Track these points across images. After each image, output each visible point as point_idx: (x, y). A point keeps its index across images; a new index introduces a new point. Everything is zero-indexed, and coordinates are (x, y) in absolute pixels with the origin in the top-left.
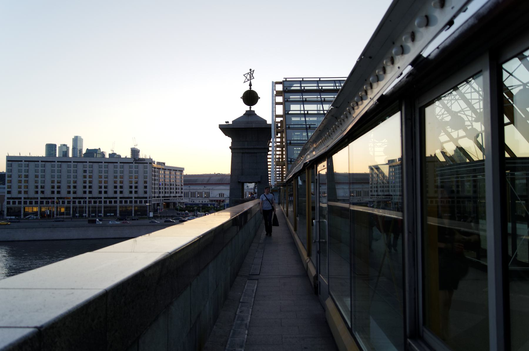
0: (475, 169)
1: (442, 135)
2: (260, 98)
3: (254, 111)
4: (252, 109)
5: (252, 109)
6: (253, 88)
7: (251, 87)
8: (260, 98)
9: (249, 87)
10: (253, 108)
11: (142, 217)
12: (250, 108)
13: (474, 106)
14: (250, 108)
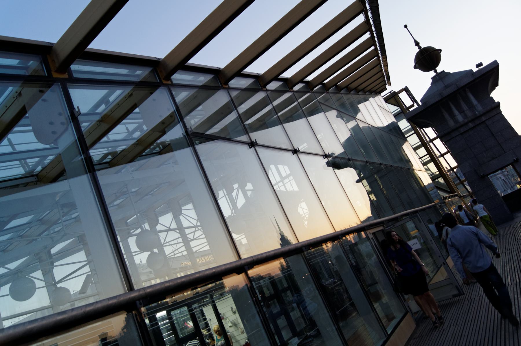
0: (153, 327)
1: (221, 198)
2: (440, 50)
3: (444, 71)
4: (438, 72)
5: (438, 72)
6: (423, 46)
7: (420, 45)
8: (440, 50)
9: (417, 47)
10: (439, 69)
11: (388, 266)
12: (436, 71)
13: (182, 241)
14: (436, 71)
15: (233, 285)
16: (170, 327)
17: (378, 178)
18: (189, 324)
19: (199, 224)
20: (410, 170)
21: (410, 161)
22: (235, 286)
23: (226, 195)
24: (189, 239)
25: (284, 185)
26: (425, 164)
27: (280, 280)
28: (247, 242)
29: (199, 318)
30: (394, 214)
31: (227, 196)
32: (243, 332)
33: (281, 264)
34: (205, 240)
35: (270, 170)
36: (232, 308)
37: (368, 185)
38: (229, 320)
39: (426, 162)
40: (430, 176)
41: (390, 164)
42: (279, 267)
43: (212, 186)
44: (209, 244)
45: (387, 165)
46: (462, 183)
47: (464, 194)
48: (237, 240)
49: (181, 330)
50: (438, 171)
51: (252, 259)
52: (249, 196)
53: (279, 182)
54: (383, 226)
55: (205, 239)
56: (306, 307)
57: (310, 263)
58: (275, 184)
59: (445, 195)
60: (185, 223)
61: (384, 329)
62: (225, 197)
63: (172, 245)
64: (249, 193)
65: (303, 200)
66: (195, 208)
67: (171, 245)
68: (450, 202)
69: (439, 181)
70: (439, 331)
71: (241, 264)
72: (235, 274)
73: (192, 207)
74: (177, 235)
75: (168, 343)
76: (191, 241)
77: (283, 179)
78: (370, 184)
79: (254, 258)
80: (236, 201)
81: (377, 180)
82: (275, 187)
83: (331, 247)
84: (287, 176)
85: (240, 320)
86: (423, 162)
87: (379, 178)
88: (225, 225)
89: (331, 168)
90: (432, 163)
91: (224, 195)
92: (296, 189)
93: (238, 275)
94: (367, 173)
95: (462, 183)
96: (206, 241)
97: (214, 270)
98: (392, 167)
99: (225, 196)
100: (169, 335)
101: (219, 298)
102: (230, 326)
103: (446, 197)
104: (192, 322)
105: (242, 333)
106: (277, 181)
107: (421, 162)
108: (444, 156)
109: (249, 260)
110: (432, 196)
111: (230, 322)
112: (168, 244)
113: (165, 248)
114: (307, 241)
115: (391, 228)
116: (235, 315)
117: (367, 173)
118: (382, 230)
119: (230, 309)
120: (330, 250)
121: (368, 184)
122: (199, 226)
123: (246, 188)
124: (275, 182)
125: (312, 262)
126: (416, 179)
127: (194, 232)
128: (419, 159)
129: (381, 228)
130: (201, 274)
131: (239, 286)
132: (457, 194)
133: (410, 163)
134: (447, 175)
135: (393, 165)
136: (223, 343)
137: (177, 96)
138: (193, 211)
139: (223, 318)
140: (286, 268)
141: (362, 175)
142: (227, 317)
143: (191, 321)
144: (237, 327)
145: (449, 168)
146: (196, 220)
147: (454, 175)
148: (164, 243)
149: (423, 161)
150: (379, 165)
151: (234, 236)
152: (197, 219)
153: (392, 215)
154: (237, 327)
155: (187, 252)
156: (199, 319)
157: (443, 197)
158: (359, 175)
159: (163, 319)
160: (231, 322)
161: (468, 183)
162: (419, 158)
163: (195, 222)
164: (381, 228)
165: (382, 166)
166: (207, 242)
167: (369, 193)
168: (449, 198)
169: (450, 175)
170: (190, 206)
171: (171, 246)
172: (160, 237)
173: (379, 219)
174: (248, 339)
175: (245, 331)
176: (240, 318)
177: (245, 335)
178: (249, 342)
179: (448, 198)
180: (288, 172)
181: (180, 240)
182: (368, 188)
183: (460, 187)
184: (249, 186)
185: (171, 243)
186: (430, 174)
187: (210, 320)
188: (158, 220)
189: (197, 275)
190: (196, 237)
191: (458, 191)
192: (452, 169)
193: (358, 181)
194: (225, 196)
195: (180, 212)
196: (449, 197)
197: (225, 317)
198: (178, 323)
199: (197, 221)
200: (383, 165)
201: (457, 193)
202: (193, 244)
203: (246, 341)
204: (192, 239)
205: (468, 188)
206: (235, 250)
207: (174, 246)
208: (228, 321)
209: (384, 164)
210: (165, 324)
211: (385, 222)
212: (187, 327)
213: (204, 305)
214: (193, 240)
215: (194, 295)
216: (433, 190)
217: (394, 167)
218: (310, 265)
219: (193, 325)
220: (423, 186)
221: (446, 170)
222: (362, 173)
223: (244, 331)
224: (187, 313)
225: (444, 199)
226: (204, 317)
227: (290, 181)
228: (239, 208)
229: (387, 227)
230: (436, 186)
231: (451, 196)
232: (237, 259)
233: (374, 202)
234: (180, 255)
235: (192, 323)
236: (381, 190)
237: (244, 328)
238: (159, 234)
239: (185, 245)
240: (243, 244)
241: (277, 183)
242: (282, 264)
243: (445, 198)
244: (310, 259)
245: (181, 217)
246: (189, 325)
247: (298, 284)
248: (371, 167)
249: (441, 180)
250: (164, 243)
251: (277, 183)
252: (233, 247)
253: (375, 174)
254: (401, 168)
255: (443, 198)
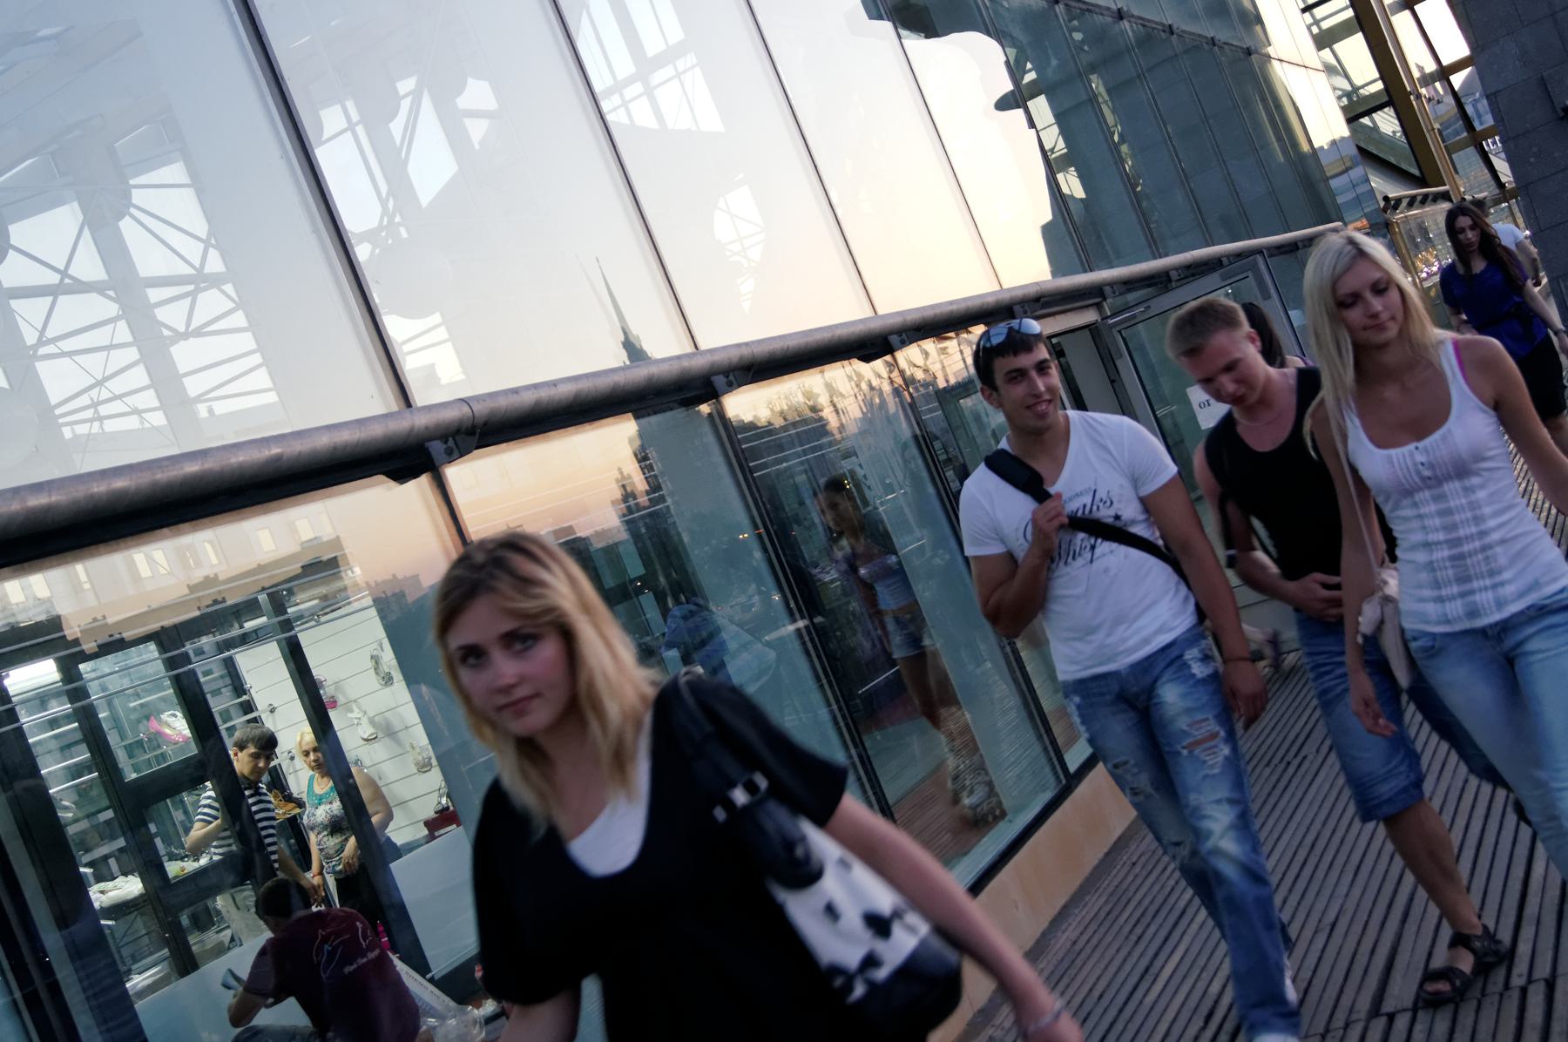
15: (394, 575)
16: (79, 736)
17: (1102, 90)
18: (169, 726)
19: (215, 264)
20: (1253, 57)
21: (1259, 19)
22: (400, 576)
23: (358, 123)
24: (166, 332)
25: (649, 92)
26: (1325, 40)
27: (611, 551)
28: (462, 377)
29: (227, 716)
30: (1155, 258)
31: (360, 130)
32: (423, 767)
33: (624, 486)
34: (247, 341)
35: (585, 14)
36: (376, 660)
37: (1053, 120)
38: (359, 708)
39: (1331, 30)
40: (1339, 98)
41: (1165, 22)
42: (613, 498)
43: (301, 114)
44: (266, 363)
45: (1149, 21)
46: (1476, 140)
47: (1481, 192)
48: (406, 348)
49: (130, 750)
50: (1382, 78)
51: (466, 410)
52: (477, 147)
53: (630, 81)
54: (1098, 306)
55: (249, 335)
56: (722, 665)
57: (752, 474)
58: (609, 92)
59: (1395, 191)
60: (149, 259)
61: (1056, 754)
62: (349, 134)
63: (77, 358)
64: (477, 130)
65: (741, 176)
66: (198, 183)
67: (70, 354)
68: (1413, 225)
69: (1376, 128)
70: (1283, 766)
71: (412, 428)
72: (381, 478)
73: (186, 180)
74: (106, 308)
75: (66, 803)
76: (177, 342)
77: (645, 65)
78: (1062, 118)
79: (477, 408)
80: (403, 156)
81: (1100, 100)
82: (606, 106)
83: (861, 415)
84: (669, 56)
85: (410, 714)
86: (1319, 28)
87: (1109, 91)
88: (276, 90)
89: (887, 26)
90: (1360, 35)
91: (345, 125)
92: (711, 121)
93: (392, 483)
94: (1054, 62)
95: (1476, 140)
96: (253, 345)
97: (275, 451)
98: (1172, 33)
99: (351, 127)
100: (66, 748)
101: (314, 617)
102: (365, 737)
103: (1398, 201)
104: (185, 717)
105: (424, 767)
106: (620, 78)
107: (1309, 28)
108: (1416, 7)
109: (451, 415)
110: (1340, 200)
111: (365, 721)
112: (50, 349)
113: (41, 367)
114: (739, 346)
115: (1134, 317)
116: (388, 690)
117: (1054, 62)
118: (1090, 328)
119: (370, 664)
120: (852, 429)
121: (1057, 116)
122: (214, 281)
123: (463, 102)
124: (609, 82)
125: (764, 466)
126: (1279, 106)
127: (193, 295)
128: (1304, 10)
129: (1090, 316)
130: (211, 464)
131: (421, 577)
132: (1448, 192)
133: (1258, 28)
134: (1419, 96)
135: (1175, 26)
136: (336, 812)
137: (580, 829)
138: (189, 195)
139: (334, 704)
140: (643, 500)
141: (1030, 77)
142: (353, 697)
143: (180, 715)
144: (399, 742)
145: (1430, 67)
146: (199, 239)
147: (1450, 100)
148: (41, 342)
149: (1317, 22)
150: (1109, 19)
151: (395, 326)
152: (204, 237)
153: (1147, 260)
154: (399, 742)
155: (159, 397)
156: (225, 722)
157: (1386, 199)
158: (1015, 71)
159: (41, 698)
160: (372, 722)
161: (1506, 149)
162: (1302, 6)
163: (193, 250)
164: (1090, 316)
165: (1125, 24)
166: (260, 349)
167: (1052, 168)
168: (1411, 205)
169: (1429, 100)
170: (175, 172)
171: (67, 360)
172: (19, 319)
173: (1085, 271)
174: (449, 796)
175: (434, 762)
176: (420, 727)
177: (435, 778)
178: (451, 808)
179: (1405, 203)
180: (676, 34)
181: (123, 332)
182: (1053, 138)
183: (1467, 159)
184: (477, 94)
185: (67, 345)
186: (1340, 93)
187: (272, 711)
188: (6, 235)
189: (192, 468)
190: (198, 325)
191: (1456, 176)
192: (1444, 73)
193: (1004, 104)
194: (351, 127)
195: (123, 204)
196: (1412, 202)
197: (341, 699)
198: (115, 718)
199: (207, 245)
200: (1130, 21)
201: (1447, 188)
202: (185, 355)
203: (440, 803)
204: (182, 329)
205: (1502, 167)
206: (386, 362)
207: (95, 362)
208: (356, 714)
209: (1133, 16)
210: (53, 723)
211: (1107, 290)
212: (156, 739)
213: (245, 640)
214: (185, 336)
215: (192, 588)
216: (1346, 171)
217: (1178, 35)
218: (754, 478)
219: (187, 732)
220: (1305, 148)
221: (1416, 74)
222: (1029, 66)
223: (430, 759)
224: (158, 668)
225: (1385, 210)
226: (245, 698)
227: (678, 75)
228: (425, 199)
229: (1114, 315)
230: (1360, 149)
231: (1419, 198)
232: (395, 408)
233: (1072, 206)
234: (132, 423)
235: (184, 722)
236: (1115, 149)
237: (430, 746)
238: (14, 304)
239: (145, 359)
240: (443, 382)
241: (618, 87)
242: (629, 489)
243: (1392, 204)
244: (755, 453)
245: (126, 225)
246: (168, 731)
247: (681, 540)
248: (1078, 36)
249: (1387, 122)
250: (41, 342)
251: (618, 87)
252: (376, 351)
253: (1093, 68)
254: (1213, 42)
255: (1382, 204)
